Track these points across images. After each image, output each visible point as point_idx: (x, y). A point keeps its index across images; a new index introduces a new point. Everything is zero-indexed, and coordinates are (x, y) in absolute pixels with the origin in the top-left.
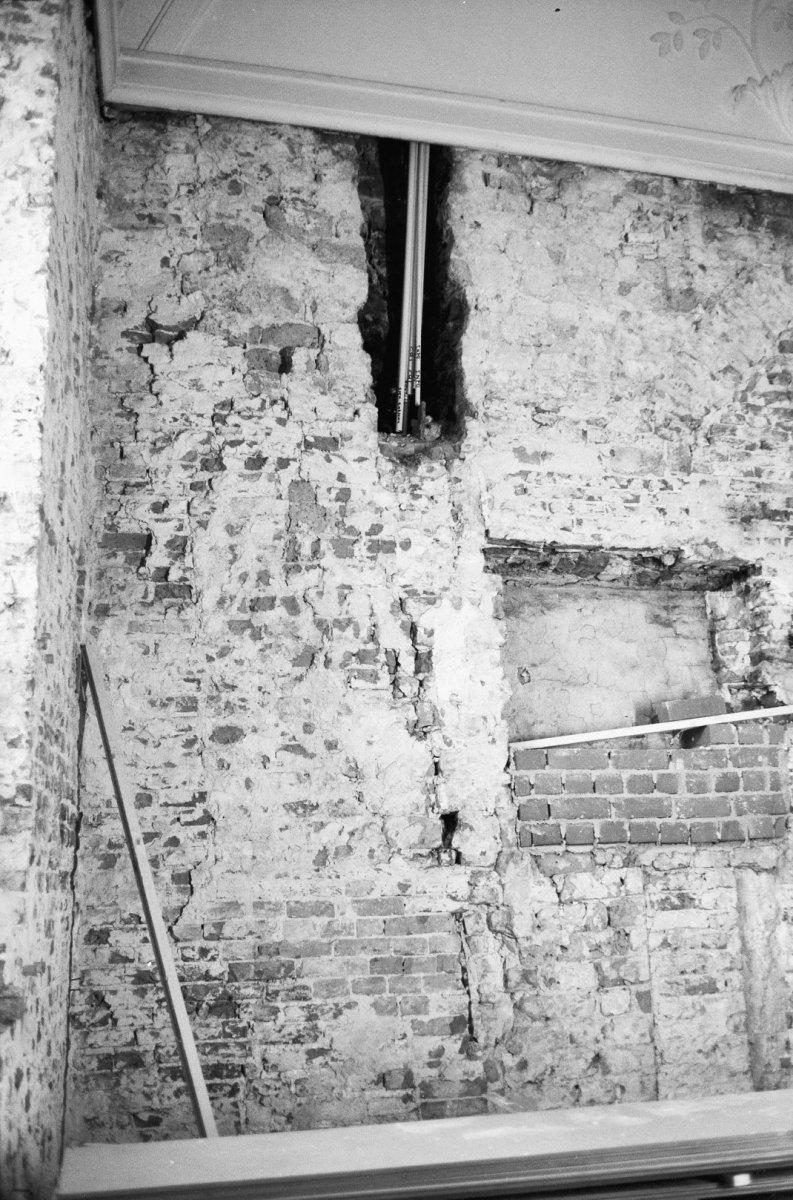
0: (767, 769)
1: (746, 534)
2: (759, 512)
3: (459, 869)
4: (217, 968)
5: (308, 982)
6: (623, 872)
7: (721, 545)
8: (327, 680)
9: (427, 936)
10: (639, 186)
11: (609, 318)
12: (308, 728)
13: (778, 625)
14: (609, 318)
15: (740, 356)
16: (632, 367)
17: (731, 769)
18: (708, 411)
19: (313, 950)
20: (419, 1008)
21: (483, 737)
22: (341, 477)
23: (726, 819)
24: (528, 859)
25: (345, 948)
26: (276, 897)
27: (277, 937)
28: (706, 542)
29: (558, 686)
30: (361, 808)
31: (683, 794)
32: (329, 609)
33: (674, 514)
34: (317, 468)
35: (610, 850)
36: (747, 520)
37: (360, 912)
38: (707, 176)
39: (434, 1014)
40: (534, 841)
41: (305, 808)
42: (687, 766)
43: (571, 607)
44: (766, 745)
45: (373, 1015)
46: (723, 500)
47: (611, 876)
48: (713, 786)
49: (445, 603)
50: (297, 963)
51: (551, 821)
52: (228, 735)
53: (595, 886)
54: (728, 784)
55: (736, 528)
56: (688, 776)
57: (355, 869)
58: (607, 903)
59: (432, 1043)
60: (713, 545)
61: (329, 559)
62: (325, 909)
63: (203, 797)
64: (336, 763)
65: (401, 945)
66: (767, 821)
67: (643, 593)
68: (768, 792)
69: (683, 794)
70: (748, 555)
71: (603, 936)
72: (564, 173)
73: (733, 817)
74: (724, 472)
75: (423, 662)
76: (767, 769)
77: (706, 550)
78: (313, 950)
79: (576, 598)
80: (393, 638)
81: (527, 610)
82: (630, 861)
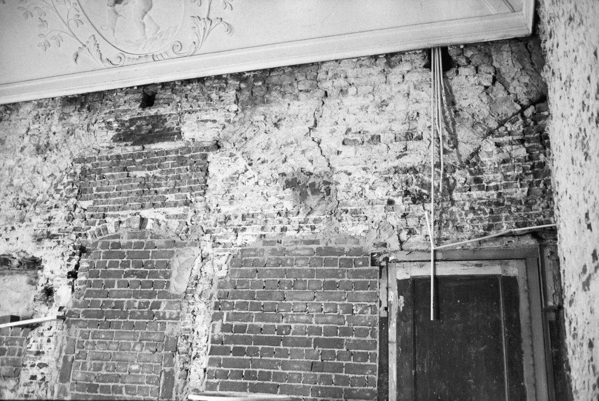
7: (27, 252)
13: (40, 285)
16: (15, 182)
28: (22, 251)
36: (39, 240)
55: (34, 244)
67: (29, 272)
70: (37, 255)
77: (22, 254)
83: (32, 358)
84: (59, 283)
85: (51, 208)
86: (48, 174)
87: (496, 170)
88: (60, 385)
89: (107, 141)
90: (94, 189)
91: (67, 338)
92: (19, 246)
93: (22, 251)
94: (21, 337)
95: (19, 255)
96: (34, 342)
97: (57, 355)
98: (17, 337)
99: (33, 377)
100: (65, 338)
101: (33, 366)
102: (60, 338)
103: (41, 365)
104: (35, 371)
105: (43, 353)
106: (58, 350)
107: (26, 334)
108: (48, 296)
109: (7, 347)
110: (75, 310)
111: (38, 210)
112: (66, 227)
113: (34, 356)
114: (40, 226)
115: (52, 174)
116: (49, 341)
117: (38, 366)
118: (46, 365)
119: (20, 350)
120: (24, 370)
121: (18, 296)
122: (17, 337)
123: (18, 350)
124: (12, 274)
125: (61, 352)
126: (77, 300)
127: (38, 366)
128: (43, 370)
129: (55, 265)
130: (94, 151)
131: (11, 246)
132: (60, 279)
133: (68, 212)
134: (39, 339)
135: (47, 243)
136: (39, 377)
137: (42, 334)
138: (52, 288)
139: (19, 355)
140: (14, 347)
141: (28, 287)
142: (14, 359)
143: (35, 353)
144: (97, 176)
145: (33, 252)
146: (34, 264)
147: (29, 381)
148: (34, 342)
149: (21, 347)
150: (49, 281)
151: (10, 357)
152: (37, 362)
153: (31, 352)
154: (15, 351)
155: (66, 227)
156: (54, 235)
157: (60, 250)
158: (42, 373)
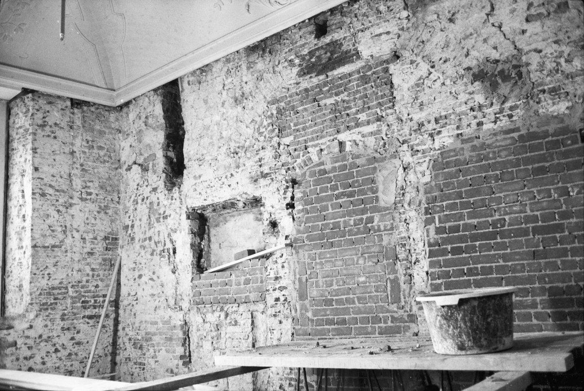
0: (259, 276)
1: (256, 186)
2: (260, 177)
3: (181, 312)
4: (140, 338)
5: (154, 342)
6: (220, 313)
7: (248, 193)
8: (156, 258)
9: (176, 331)
10: (228, 60)
11: (217, 118)
12: (154, 273)
13: (265, 219)
14: (217, 118)
15: (256, 114)
16: (224, 134)
17: (248, 276)
18: (245, 141)
19: (155, 334)
20: (174, 352)
21: (186, 272)
22: (158, 199)
23: (246, 295)
24: (195, 309)
25: (160, 334)
26: (148, 320)
27: (149, 330)
28: (244, 193)
29: (229, 248)
30: (163, 295)
31: (234, 287)
32: (156, 238)
33: (234, 185)
34: (153, 198)
35: (216, 305)
36: (256, 181)
37: (163, 324)
38: (245, 45)
39: (177, 354)
40: (198, 304)
41: (153, 295)
42: (236, 276)
43: (233, 219)
44: (259, 267)
45: (165, 353)
46: (248, 175)
47: (217, 314)
48: (242, 283)
49: (178, 232)
50: (152, 337)
51: (201, 297)
52: (140, 276)
53: (212, 318)
54: (247, 282)
55: (252, 185)
56: (236, 280)
57: (161, 312)
58: (216, 323)
59: (176, 362)
60: (246, 194)
61: (156, 224)
62: (156, 323)
63: (136, 294)
64: (158, 282)
65: (171, 334)
66: (258, 295)
67: (253, 210)
68: (259, 284)
69: (234, 287)
70: (257, 194)
71: (214, 334)
72: (209, 66)
73: (248, 294)
74: (249, 163)
75: (174, 252)
76: (259, 276)
77: (244, 196)
78: (155, 334)
79: (233, 216)
80: (169, 245)
81: (221, 224)
82: (222, 309)
91: (298, 262)
92: (240, 189)
97: (292, 278)
99: (277, 299)
103: (282, 288)
104: (278, 294)
106: (292, 273)
116: (283, 267)
118: (285, 288)
120: (268, 294)
128: (283, 292)
132: (280, 211)
134: (275, 266)
135: (262, 182)
136: (282, 299)
139: (262, 282)
143: (274, 279)
146: (256, 202)
156: (267, 174)
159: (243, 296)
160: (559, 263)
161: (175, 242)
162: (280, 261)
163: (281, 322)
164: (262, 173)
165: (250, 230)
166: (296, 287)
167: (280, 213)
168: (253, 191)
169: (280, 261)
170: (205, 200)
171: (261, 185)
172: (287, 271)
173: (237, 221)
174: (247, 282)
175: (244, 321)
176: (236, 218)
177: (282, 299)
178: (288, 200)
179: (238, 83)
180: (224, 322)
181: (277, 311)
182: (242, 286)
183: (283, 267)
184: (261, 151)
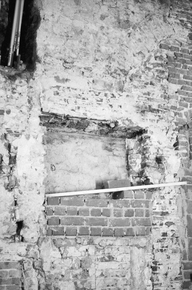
0: (144, 209)
1: (142, 117)
2: (148, 109)
3: (23, 244)
7: (133, 121)
9: (8, 270)
13: (152, 153)
16: (103, 48)
17: (131, 208)
18: (131, 68)
23: (128, 227)
24: (50, 241)
28: (127, 119)
29: (66, 172)
31: (112, 217)
33: (115, 107)
36: (143, 112)
43: (73, 141)
46: (135, 104)
47: (83, 248)
51: (60, 226)
54: (129, 214)
55: (139, 115)
56: (115, 210)
60: (130, 121)
67: (102, 138)
69: (112, 217)
70: (143, 125)
73: (131, 226)
74: (136, 92)
77: (127, 122)
79: (75, 138)
81: (56, 142)
83: (160, 218)
84: (168, 153)
85: (147, 84)
86: (138, 51)
87: (146, 70)
88: (189, 239)
89: (185, 37)
90: (181, 76)
91: (186, 201)
92: (125, 115)
93: (127, 119)
94: (145, 199)
95: (123, 123)
96: (158, 204)
97: (181, 214)
98: (141, 199)
99: (165, 234)
100: (185, 201)
101: (161, 225)
102: (180, 200)
103: (169, 224)
104: (165, 229)
105: (167, 213)
106: (180, 210)
107: (149, 197)
108: (158, 163)
109: (134, 209)
110: (188, 178)
111: (135, 83)
112: (164, 105)
113: (161, 216)
114: (140, 98)
115: (140, 53)
116: (170, 203)
117: (166, 224)
118: (172, 223)
119: (147, 211)
120: (155, 228)
121: (95, 160)
122: (141, 199)
123: (145, 212)
124: (83, 138)
125: (183, 212)
126: (187, 169)
127: (166, 224)
128: (172, 227)
129: (160, 138)
130: (177, 42)
131: (115, 113)
132: (169, 149)
133: (163, 91)
134: (162, 201)
135: (150, 115)
136: (170, 234)
137: (163, 197)
138: (161, 157)
139: (147, 215)
140: (141, 208)
141: (106, 153)
142: (144, 219)
143: (161, 213)
144: (182, 65)
145: (138, 122)
146: (138, 133)
147: (162, 238)
148: (158, 204)
149: (147, 209)
150: (159, 150)
151: (139, 218)
152: (164, 222)
153: (157, 213)
154: (142, 213)
155: (164, 105)
156: (154, 110)
157: (163, 124)
158: (172, 231)
159: (125, 228)
160: (89, 229)
161: (16, 148)
162: (167, 197)
163: (169, 258)
164: (150, 106)
165: (97, 158)
166: (185, 223)
167: (168, 151)
168: (139, 122)
169: (167, 197)
170: (73, 110)
171: (148, 118)
172: (176, 208)
173: (79, 144)
174: (129, 214)
175: (122, 256)
176: (77, 140)
177: (170, 234)
178: (174, 141)
179: (122, 8)
180: (94, 258)
181: (165, 245)
182: (123, 218)
183: (170, 203)
184: (149, 85)
